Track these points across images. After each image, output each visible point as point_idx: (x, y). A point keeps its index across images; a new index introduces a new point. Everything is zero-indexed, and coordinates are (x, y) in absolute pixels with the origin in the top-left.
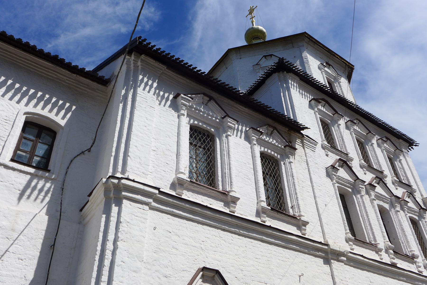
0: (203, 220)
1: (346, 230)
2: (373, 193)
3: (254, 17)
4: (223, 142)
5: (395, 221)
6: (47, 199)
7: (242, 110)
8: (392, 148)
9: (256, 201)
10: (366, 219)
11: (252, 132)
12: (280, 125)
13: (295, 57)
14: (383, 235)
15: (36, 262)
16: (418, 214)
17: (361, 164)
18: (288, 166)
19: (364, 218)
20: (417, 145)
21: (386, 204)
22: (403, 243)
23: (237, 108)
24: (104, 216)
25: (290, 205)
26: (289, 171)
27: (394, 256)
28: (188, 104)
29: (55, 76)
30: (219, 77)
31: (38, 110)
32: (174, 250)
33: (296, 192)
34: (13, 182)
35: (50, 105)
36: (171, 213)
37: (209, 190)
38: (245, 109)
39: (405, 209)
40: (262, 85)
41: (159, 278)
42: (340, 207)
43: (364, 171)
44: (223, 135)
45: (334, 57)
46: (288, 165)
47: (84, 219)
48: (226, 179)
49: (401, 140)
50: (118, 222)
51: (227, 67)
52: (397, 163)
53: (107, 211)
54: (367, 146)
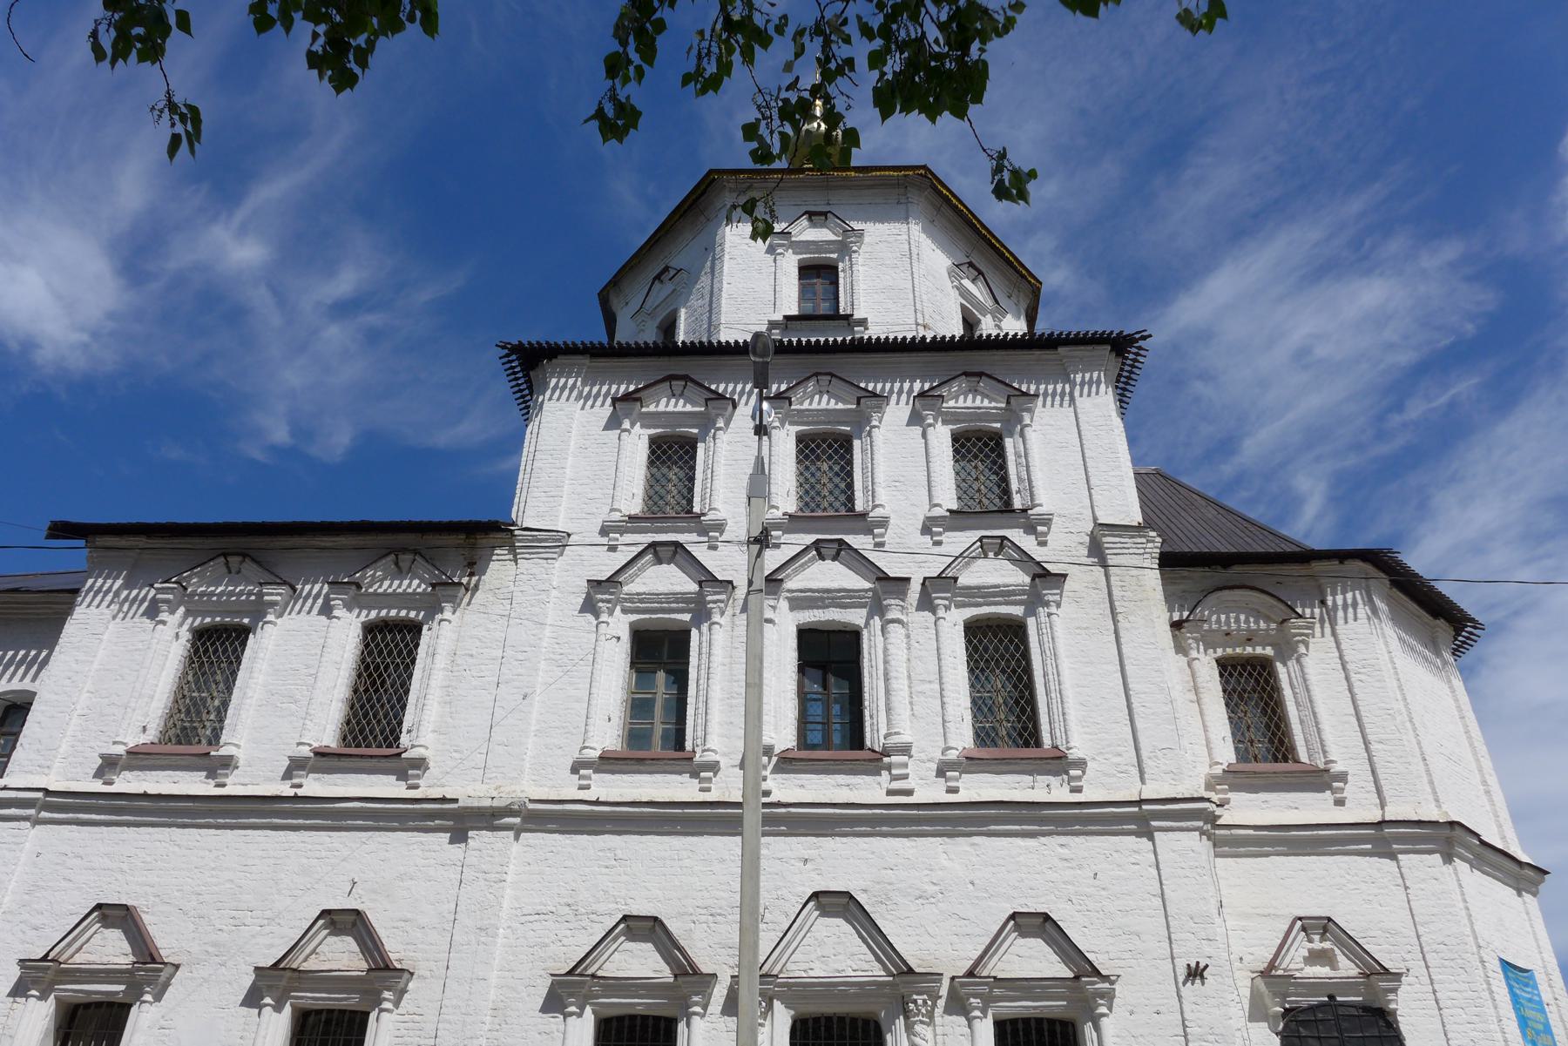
12: (440, 535)
21: (857, 610)
41: (24, 932)
49: (1061, 350)
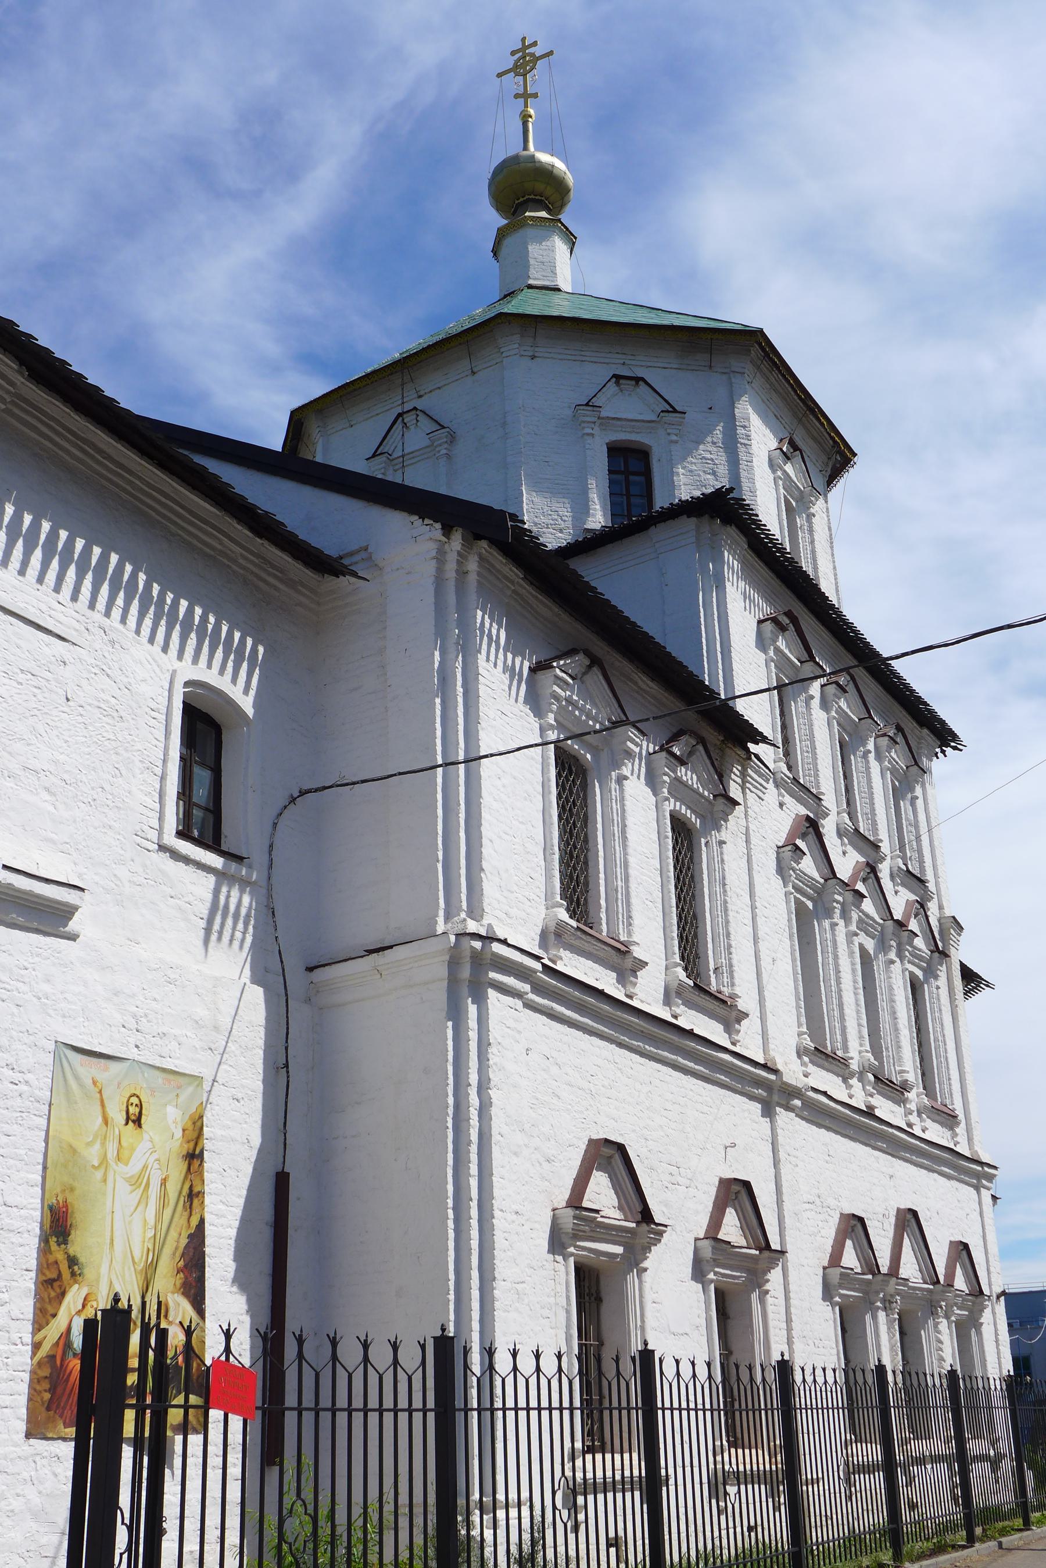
0: (595, 1025)
1: (800, 1025)
2: (855, 916)
3: (535, 96)
4: (611, 795)
5: (881, 988)
6: (249, 939)
7: (644, 687)
8: (902, 758)
9: (664, 963)
10: (833, 988)
11: (664, 761)
13: (711, 408)
14: (860, 1032)
15: (258, 1104)
16: (925, 965)
17: (842, 826)
18: (715, 853)
19: (831, 986)
20: (959, 746)
22: (887, 1049)
23: (636, 683)
24: (450, 1024)
25: (712, 966)
26: (717, 869)
27: (873, 1088)
28: (563, 694)
29: (219, 547)
30: (434, 390)
31: (223, 683)
32: (555, 1101)
33: (727, 930)
34: (191, 898)
35: (221, 647)
36: (548, 1011)
37: (599, 945)
38: (649, 682)
39: (907, 953)
40: (634, 534)
42: (794, 960)
43: (843, 844)
44: (611, 776)
45: (811, 417)
46: (715, 848)
47: (318, 992)
48: (617, 906)
50: (483, 1044)
51: (475, 370)
52: (905, 804)
53: (456, 1013)
54: (852, 757)
